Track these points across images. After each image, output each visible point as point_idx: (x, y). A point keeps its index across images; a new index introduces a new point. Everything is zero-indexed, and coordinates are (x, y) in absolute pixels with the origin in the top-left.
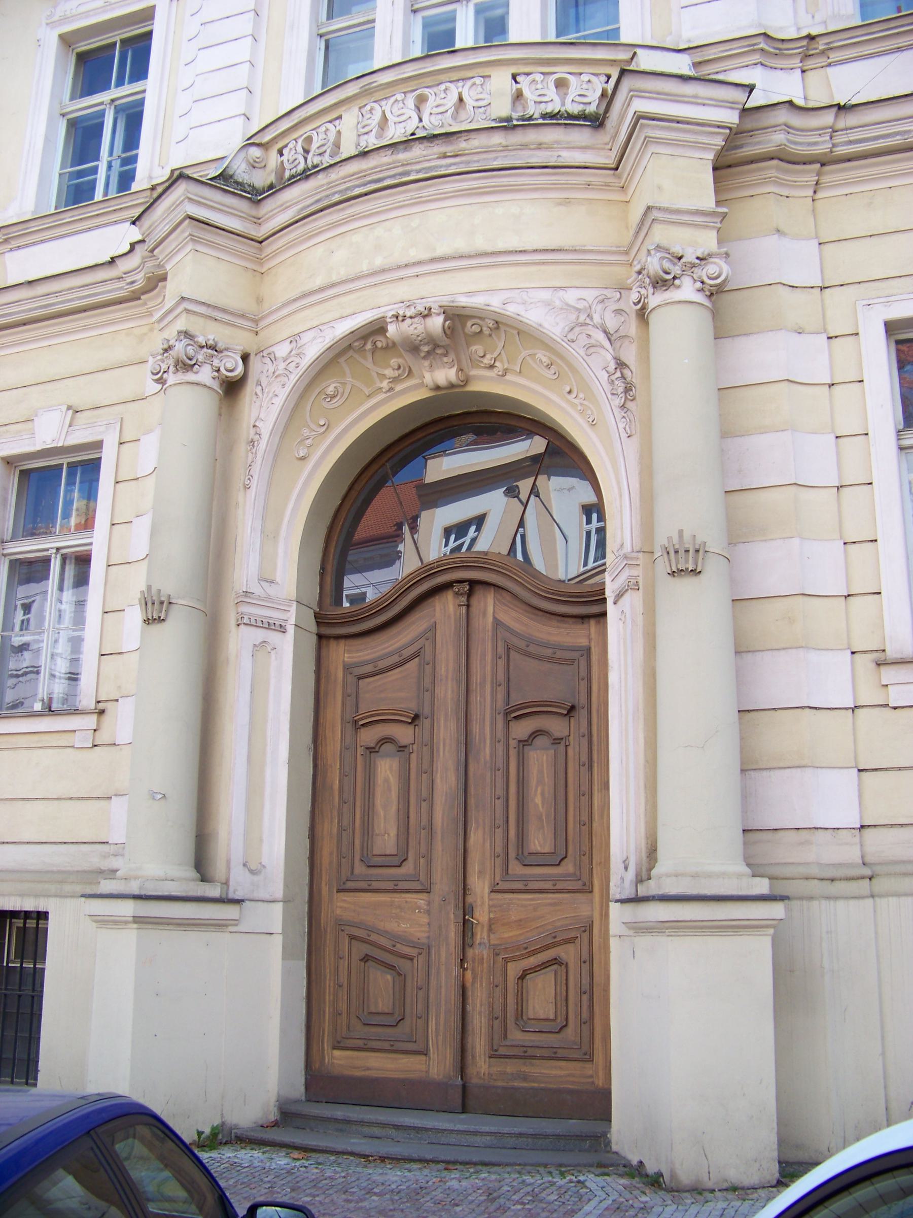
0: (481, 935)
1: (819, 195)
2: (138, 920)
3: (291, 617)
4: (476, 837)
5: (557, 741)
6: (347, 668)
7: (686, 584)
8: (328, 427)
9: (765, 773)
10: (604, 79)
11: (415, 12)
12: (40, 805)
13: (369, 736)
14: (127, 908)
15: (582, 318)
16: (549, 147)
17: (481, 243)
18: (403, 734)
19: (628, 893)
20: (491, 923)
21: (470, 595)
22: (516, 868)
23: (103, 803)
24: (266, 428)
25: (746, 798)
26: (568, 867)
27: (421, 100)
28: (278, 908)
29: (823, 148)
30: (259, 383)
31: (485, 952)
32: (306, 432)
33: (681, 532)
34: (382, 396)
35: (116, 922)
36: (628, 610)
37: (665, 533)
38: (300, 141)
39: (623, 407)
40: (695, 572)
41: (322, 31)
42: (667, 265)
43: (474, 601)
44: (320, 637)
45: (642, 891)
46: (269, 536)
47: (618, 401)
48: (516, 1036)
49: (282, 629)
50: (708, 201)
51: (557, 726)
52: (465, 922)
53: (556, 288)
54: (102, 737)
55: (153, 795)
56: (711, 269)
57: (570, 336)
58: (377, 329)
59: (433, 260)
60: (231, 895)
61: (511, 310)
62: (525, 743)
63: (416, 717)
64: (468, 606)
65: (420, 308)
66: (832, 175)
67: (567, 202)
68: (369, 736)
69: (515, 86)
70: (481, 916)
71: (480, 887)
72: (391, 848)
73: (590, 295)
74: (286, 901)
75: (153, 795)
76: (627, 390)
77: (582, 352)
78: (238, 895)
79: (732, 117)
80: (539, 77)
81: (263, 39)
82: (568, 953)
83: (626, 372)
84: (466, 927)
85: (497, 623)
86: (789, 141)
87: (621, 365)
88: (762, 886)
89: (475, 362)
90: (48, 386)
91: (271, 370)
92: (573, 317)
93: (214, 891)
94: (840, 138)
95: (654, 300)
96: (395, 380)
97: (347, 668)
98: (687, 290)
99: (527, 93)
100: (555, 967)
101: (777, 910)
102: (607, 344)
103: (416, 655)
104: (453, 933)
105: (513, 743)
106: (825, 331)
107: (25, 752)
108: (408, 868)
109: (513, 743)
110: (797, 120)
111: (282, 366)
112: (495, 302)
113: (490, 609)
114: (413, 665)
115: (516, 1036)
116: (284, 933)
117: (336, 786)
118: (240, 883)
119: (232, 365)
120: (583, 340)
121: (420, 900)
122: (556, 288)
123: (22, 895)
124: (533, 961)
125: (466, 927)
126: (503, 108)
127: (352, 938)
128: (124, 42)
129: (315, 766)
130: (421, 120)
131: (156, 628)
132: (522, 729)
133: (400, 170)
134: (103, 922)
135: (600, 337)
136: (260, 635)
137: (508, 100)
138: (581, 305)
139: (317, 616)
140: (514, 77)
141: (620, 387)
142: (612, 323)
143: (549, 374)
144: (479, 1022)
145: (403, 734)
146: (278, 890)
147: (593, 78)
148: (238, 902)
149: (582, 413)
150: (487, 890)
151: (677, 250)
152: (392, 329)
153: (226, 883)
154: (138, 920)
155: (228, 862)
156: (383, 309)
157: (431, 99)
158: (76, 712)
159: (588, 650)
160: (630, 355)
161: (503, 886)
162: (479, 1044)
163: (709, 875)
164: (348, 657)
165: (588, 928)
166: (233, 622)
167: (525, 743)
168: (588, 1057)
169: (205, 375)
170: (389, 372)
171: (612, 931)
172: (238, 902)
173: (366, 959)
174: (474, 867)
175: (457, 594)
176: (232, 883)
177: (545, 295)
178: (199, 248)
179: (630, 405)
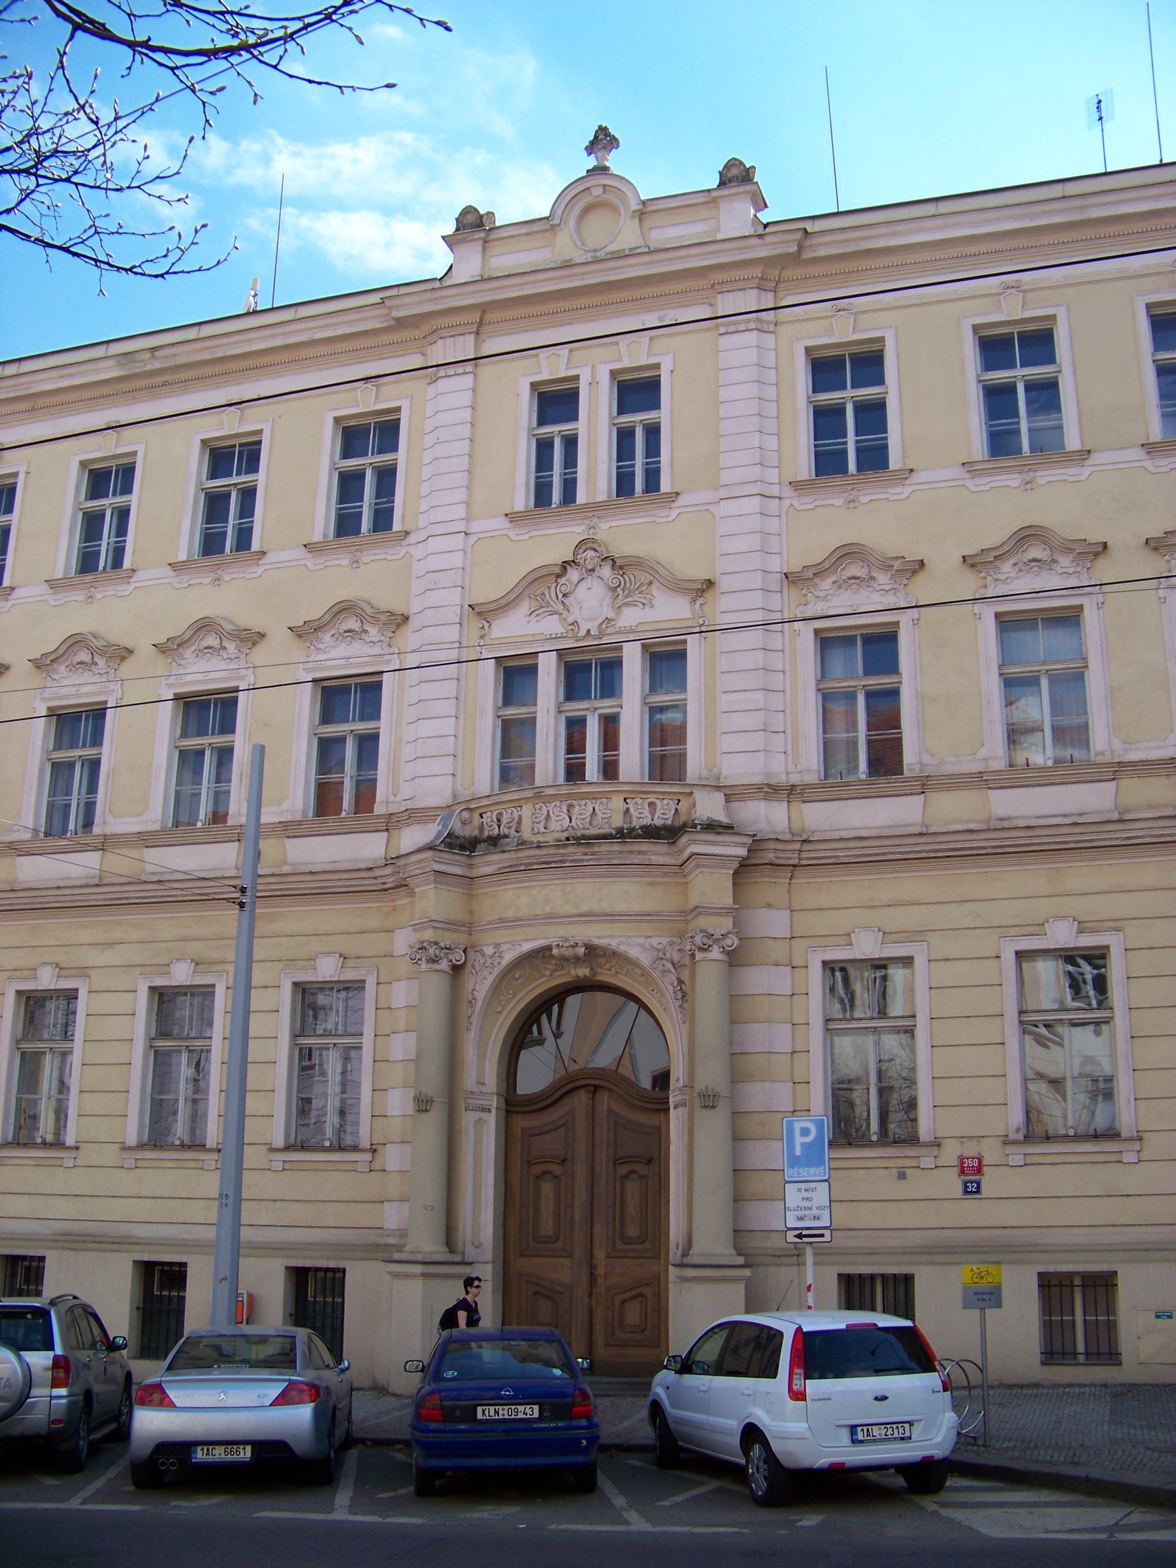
0: (600, 1281)
1: (794, 881)
2: (424, 1275)
3: (494, 1102)
4: (597, 1228)
5: (642, 1177)
6: (524, 1130)
7: (710, 1112)
8: (515, 994)
9: (748, 1203)
10: (676, 802)
11: (560, 712)
12: (335, 1205)
13: (536, 1170)
14: (418, 1269)
15: (661, 955)
16: (645, 853)
17: (606, 907)
18: (557, 1169)
19: (678, 1260)
20: (606, 1276)
21: (594, 1092)
22: (619, 1245)
23: (378, 1205)
24: (481, 995)
25: (736, 1215)
26: (648, 1245)
27: (570, 807)
28: (490, 1265)
29: (795, 862)
30: (473, 967)
31: (603, 1291)
32: (502, 997)
33: (706, 1087)
34: (545, 978)
35: (410, 1276)
36: (680, 1115)
37: (699, 1086)
38: (495, 813)
39: (681, 1006)
40: (713, 1107)
41: (500, 714)
42: (705, 941)
43: (597, 1095)
44: (507, 1111)
45: (685, 1261)
46: (481, 1057)
47: (678, 1003)
48: (619, 1335)
49: (489, 1111)
50: (728, 901)
51: (642, 1169)
52: (592, 1273)
53: (647, 937)
54: (377, 1165)
55: (426, 1207)
56: (729, 942)
57: (655, 966)
58: (549, 948)
59: (579, 915)
60: (466, 1260)
61: (623, 948)
62: (626, 1176)
63: (564, 1161)
64: (593, 1099)
65: (572, 943)
66: (799, 872)
67: (652, 884)
68: (536, 1170)
69: (626, 806)
70: (601, 1270)
71: (600, 1254)
72: (550, 1233)
73: (665, 940)
74: (493, 1262)
75: (426, 1207)
76: (683, 997)
77: (660, 975)
78: (470, 1260)
79: (743, 852)
80: (640, 801)
81: (462, 717)
82: (647, 1291)
83: (683, 986)
84: (592, 1276)
85: (610, 1110)
86: (777, 858)
87: (680, 982)
88: (741, 1260)
89: (599, 966)
90: (324, 938)
91: (482, 961)
92: (655, 954)
93: (458, 1258)
94: (804, 855)
95: (699, 956)
96: (555, 971)
97: (522, 1129)
98: (716, 953)
99: (632, 810)
100: (640, 1298)
101: (747, 1272)
102: (673, 971)
103: (564, 1124)
104: (585, 1279)
105: (618, 1177)
106: (791, 962)
107: (323, 1173)
108: (560, 1244)
109: (618, 1177)
110: (780, 846)
111: (489, 961)
112: (613, 943)
113: (606, 1101)
114: (562, 1131)
115: (619, 1335)
116: (493, 1280)
117: (518, 1198)
118: (471, 1253)
119: (459, 957)
120: (661, 968)
121: (567, 1262)
122: (647, 937)
123: (327, 1259)
124: (628, 1295)
125: (592, 1276)
126: (618, 821)
127: (528, 1282)
128: (241, 445)
129: (506, 1185)
130: (571, 822)
131: (423, 1116)
132: (623, 1170)
133: (560, 859)
134: (396, 1275)
135: (670, 966)
136: (476, 1115)
137: (621, 815)
138: (660, 947)
139: (506, 1100)
140: (625, 799)
141: (679, 995)
142: (676, 958)
143: (642, 979)
144: (599, 1327)
145: (557, 1169)
146: (489, 1257)
147: (671, 802)
148: (471, 1263)
149: (659, 1002)
150: (603, 1256)
151: (711, 931)
152: (555, 951)
153: (463, 1253)
154: (424, 1275)
155: (464, 1243)
156: (551, 940)
157: (577, 808)
158: (355, 1148)
159: (659, 1128)
160: (685, 977)
161: (612, 1254)
162: (599, 1340)
163: (716, 1255)
164: (523, 1124)
165: (658, 1278)
166: (463, 1109)
167: (626, 1176)
168: (657, 1345)
169: (444, 965)
170: (550, 967)
171: (670, 1280)
172: (471, 1263)
173: (536, 1293)
174: (596, 1245)
175: (587, 1092)
176: (467, 1252)
177: (641, 940)
178: (438, 886)
179: (685, 1005)
